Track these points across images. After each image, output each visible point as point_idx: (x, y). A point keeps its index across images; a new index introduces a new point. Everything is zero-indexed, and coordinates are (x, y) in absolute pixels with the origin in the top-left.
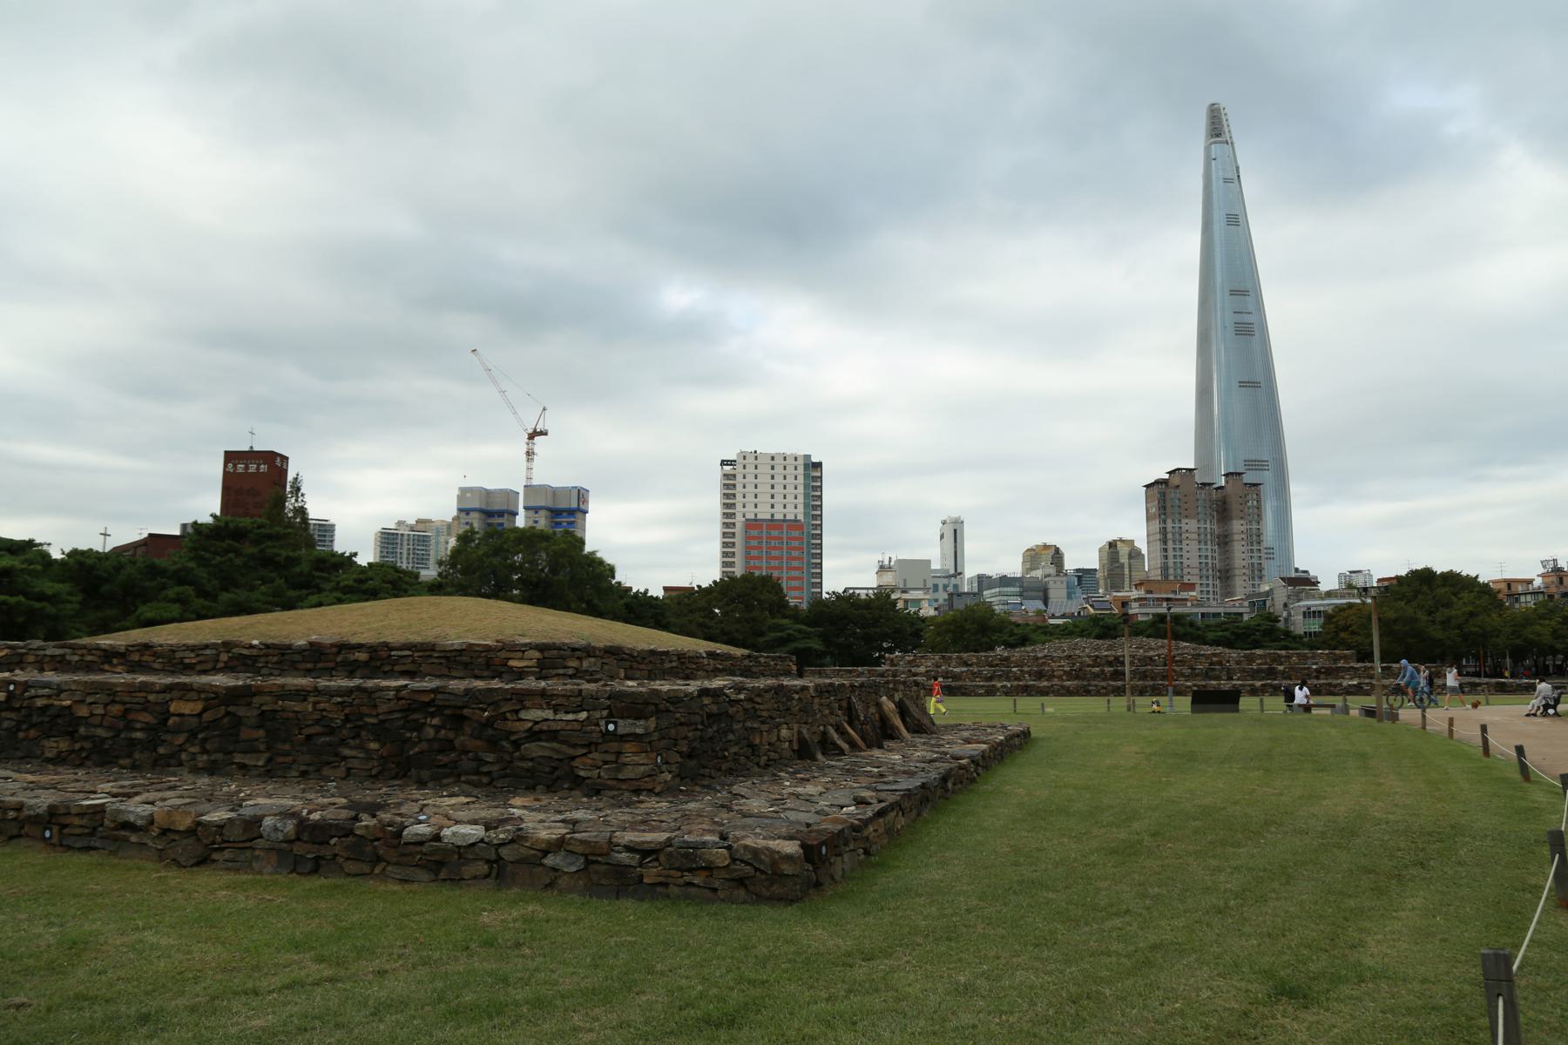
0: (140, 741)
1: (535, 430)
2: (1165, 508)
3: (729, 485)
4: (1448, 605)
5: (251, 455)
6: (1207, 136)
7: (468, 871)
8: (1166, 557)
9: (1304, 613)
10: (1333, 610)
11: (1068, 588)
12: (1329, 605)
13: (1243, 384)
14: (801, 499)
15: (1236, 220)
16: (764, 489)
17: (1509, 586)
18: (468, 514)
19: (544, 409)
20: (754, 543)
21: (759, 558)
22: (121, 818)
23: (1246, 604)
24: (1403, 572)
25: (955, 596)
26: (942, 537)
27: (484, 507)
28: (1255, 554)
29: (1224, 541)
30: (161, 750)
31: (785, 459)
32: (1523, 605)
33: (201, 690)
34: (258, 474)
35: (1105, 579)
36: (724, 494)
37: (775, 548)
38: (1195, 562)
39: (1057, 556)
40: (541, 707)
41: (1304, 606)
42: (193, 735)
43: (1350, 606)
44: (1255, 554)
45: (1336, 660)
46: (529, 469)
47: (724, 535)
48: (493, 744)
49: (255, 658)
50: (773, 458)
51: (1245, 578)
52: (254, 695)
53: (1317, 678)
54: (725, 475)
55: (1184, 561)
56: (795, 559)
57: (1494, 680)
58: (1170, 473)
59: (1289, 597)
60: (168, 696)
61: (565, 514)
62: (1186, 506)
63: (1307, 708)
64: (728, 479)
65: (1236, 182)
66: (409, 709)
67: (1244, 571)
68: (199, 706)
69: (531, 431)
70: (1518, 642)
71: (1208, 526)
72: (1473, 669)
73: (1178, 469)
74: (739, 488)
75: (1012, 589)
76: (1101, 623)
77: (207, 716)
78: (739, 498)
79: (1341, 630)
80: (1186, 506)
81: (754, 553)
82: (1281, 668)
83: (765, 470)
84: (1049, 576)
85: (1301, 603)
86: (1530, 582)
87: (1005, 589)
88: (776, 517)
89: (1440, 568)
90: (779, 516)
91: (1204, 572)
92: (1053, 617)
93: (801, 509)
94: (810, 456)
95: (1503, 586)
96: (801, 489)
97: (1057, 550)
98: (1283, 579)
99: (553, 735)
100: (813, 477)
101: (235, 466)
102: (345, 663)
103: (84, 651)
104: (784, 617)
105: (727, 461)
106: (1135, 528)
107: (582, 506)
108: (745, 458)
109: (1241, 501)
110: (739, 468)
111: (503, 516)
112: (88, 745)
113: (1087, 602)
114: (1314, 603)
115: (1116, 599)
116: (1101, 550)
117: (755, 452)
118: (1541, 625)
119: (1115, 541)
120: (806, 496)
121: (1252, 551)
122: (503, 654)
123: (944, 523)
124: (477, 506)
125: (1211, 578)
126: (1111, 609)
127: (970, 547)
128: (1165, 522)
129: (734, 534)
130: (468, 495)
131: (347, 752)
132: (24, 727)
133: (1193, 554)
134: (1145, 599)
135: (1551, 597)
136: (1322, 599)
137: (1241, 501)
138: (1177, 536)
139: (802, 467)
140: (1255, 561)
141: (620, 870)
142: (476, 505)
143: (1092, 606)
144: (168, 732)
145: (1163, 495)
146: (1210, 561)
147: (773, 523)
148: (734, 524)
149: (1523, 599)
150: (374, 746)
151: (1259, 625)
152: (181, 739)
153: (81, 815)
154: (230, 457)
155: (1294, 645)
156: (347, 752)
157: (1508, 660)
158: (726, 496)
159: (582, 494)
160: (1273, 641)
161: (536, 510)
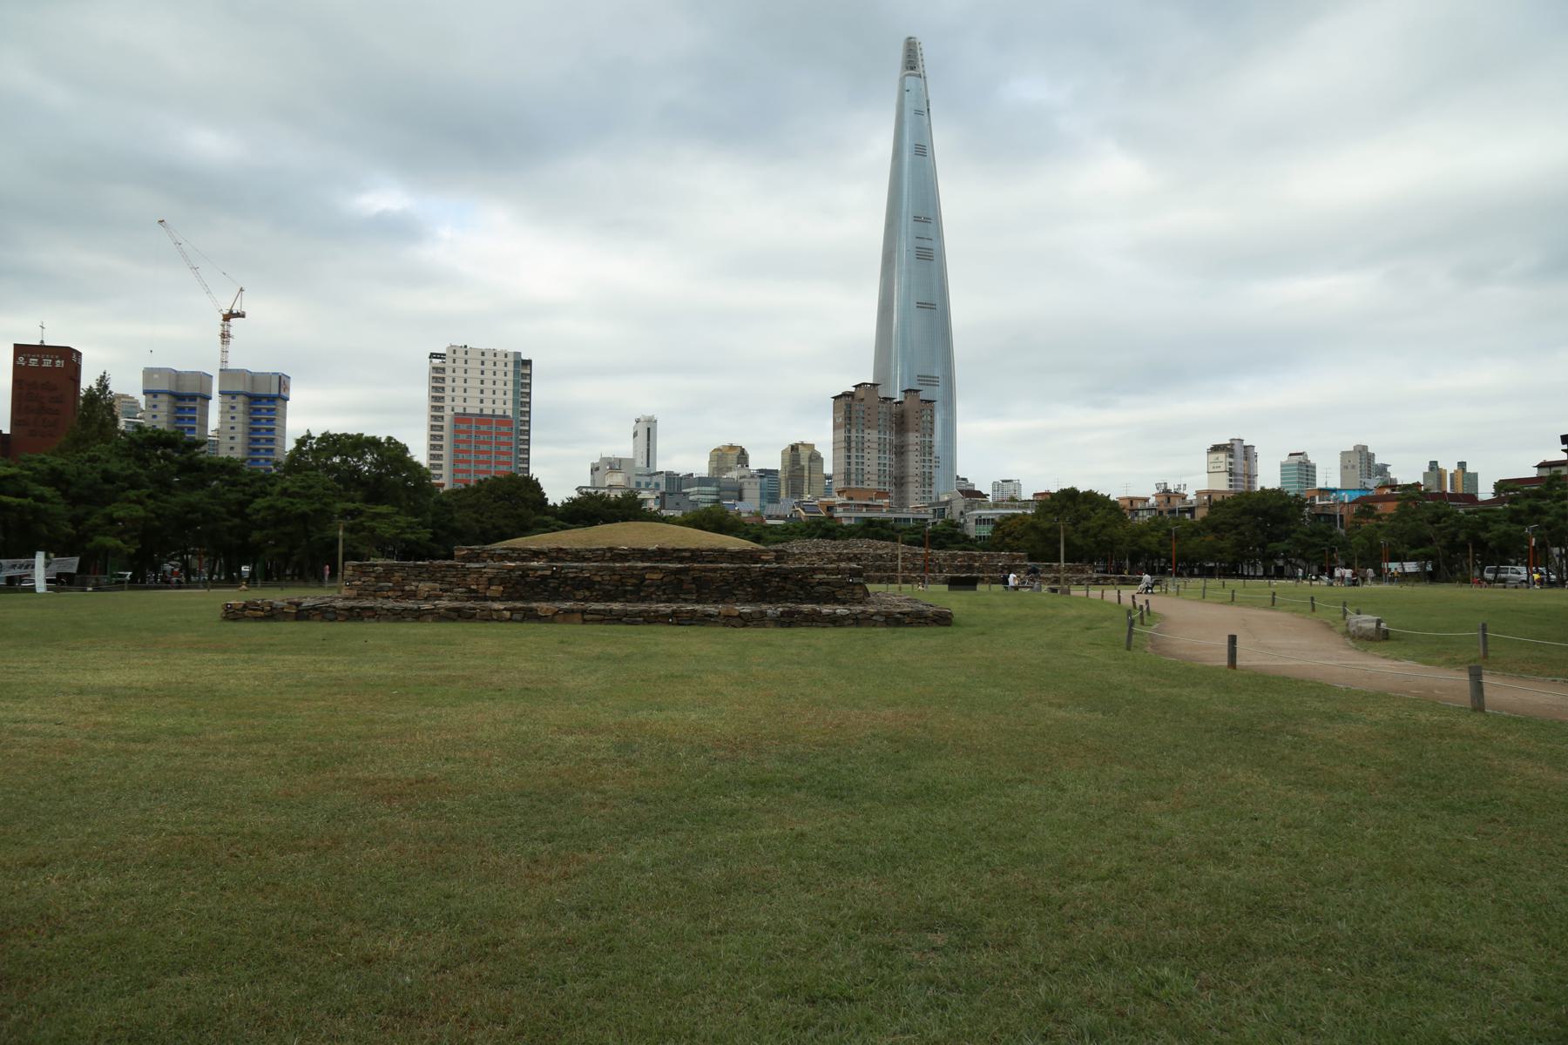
0: (631, 591)
1: (231, 312)
2: (850, 418)
3: (438, 379)
4: (1087, 518)
5: (41, 350)
6: (902, 68)
7: (846, 623)
8: (849, 464)
9: (976, 520)
10: (1000, 519)
11: (761, 489)
12: (996, 514)
13: (921, 305)
14: (510, 395)
15: (923, 150)
17: (1132, 502)
18: (155, 396)
19: (241, 290)
20: (463, 437)
21: (468, 452)
22: (707, 613)
23: (930, 511)
24: (1054, 490)
25: (666, 495)
26: (635, 435)
27: (174, 390)
28: (927, 464)
29: (900, 451)
30: (642, 594)
31: (495, 355)
33: (662, 570)
34: (53, 368)
35: (787, 480)
36: (433, 387)
37: (484, 443)
38: (874, 469)
39: (742, 457)
40: (821, 574)
41: (978, 514)
42: (658, 587)
43: (1014, 516)
44: (927, 464)
45: (1014, 559)
46: (224, 352)
47: (433, 427)
48: (801, 588)
49: (626, 555)
50: (483, 354)
51: (917, 485)
54: (434, 368)
55: (865, 467)
56: (504, 453)
57: (1118, 576)
58: (856, 386)
59: (966, 507)
60: (644, 572)
61: (264, 401)
62: (869, 418)
63: (1016, 588)
65: (926, 114)
66: (765, 575)
67: (917, 478)
68: (661, 576)
69: (226, 312)
70: (1135, 548)
71: (887, 437)
72: (1102, 569)
73: (864, 384)
74: (448, 381)
75: (709, 489)
76: (823, 526)
78: (448, 392)
80: (869, 418)
81: (463, 447)
82: (977, 564)
83: (474, 364)
84: (744, 477)
85: (974, 512)
86: (1146, 500)
87: (704, 488)
88: (485, 412)
89: (1082, 488)
90: (487, 411)
91: (882, 478)
92: (770, 517)
93: (510, 405)
94: (520, 353)
95: (1127, 503)
96: (510, 386)
97: (743, 451)
98: (961, 491)
99: (828, 584)
100: (523, 374)
101: (27, 359)
102: (677, 557)
103: (520, 552)
104: (546, 514)
106: (822, 436)
107: (283, 393)
108: (455, 352)
109: (917, 416)
110: (449, 362)
111: (195, 400)
112: (601, 593)
113: (799, 506)
114: (985, 513)
115: (822, 504)
116: (783, 453)
117: (466, 347)
118: (1153, 536)
120: (515, 392)
122: (758, 553)
123: (638, 421)
124: (167, 389)
125: (887, 483)
126: (819, 512)
127: (661, 444)
128: (849, 431)
129: (442, 427)
130: (156, 376)
131: (737, 592)
133: (874, 462)
134: (848, 505)
135: (1161, 513)
136: (991, 509)
137: (917, 416)
138: (860, 445)
140: (927, 470)
142: (166, 388)
143: (803, 509)
144: (645, 586)
145: (849, 406)
146: (887, 468)
147: (482, 418)
148: (442, 417)
149: (1141, 513)
150: (750, 589)
151: (944, 530)
152: (652, 589)
153: (687, 613)
154: (20, 350)
155: (971, 547)
156: (737, 592)
157: (1127, 561)
158: (435, 389)
159: (283, 381)
161: (233, 395)
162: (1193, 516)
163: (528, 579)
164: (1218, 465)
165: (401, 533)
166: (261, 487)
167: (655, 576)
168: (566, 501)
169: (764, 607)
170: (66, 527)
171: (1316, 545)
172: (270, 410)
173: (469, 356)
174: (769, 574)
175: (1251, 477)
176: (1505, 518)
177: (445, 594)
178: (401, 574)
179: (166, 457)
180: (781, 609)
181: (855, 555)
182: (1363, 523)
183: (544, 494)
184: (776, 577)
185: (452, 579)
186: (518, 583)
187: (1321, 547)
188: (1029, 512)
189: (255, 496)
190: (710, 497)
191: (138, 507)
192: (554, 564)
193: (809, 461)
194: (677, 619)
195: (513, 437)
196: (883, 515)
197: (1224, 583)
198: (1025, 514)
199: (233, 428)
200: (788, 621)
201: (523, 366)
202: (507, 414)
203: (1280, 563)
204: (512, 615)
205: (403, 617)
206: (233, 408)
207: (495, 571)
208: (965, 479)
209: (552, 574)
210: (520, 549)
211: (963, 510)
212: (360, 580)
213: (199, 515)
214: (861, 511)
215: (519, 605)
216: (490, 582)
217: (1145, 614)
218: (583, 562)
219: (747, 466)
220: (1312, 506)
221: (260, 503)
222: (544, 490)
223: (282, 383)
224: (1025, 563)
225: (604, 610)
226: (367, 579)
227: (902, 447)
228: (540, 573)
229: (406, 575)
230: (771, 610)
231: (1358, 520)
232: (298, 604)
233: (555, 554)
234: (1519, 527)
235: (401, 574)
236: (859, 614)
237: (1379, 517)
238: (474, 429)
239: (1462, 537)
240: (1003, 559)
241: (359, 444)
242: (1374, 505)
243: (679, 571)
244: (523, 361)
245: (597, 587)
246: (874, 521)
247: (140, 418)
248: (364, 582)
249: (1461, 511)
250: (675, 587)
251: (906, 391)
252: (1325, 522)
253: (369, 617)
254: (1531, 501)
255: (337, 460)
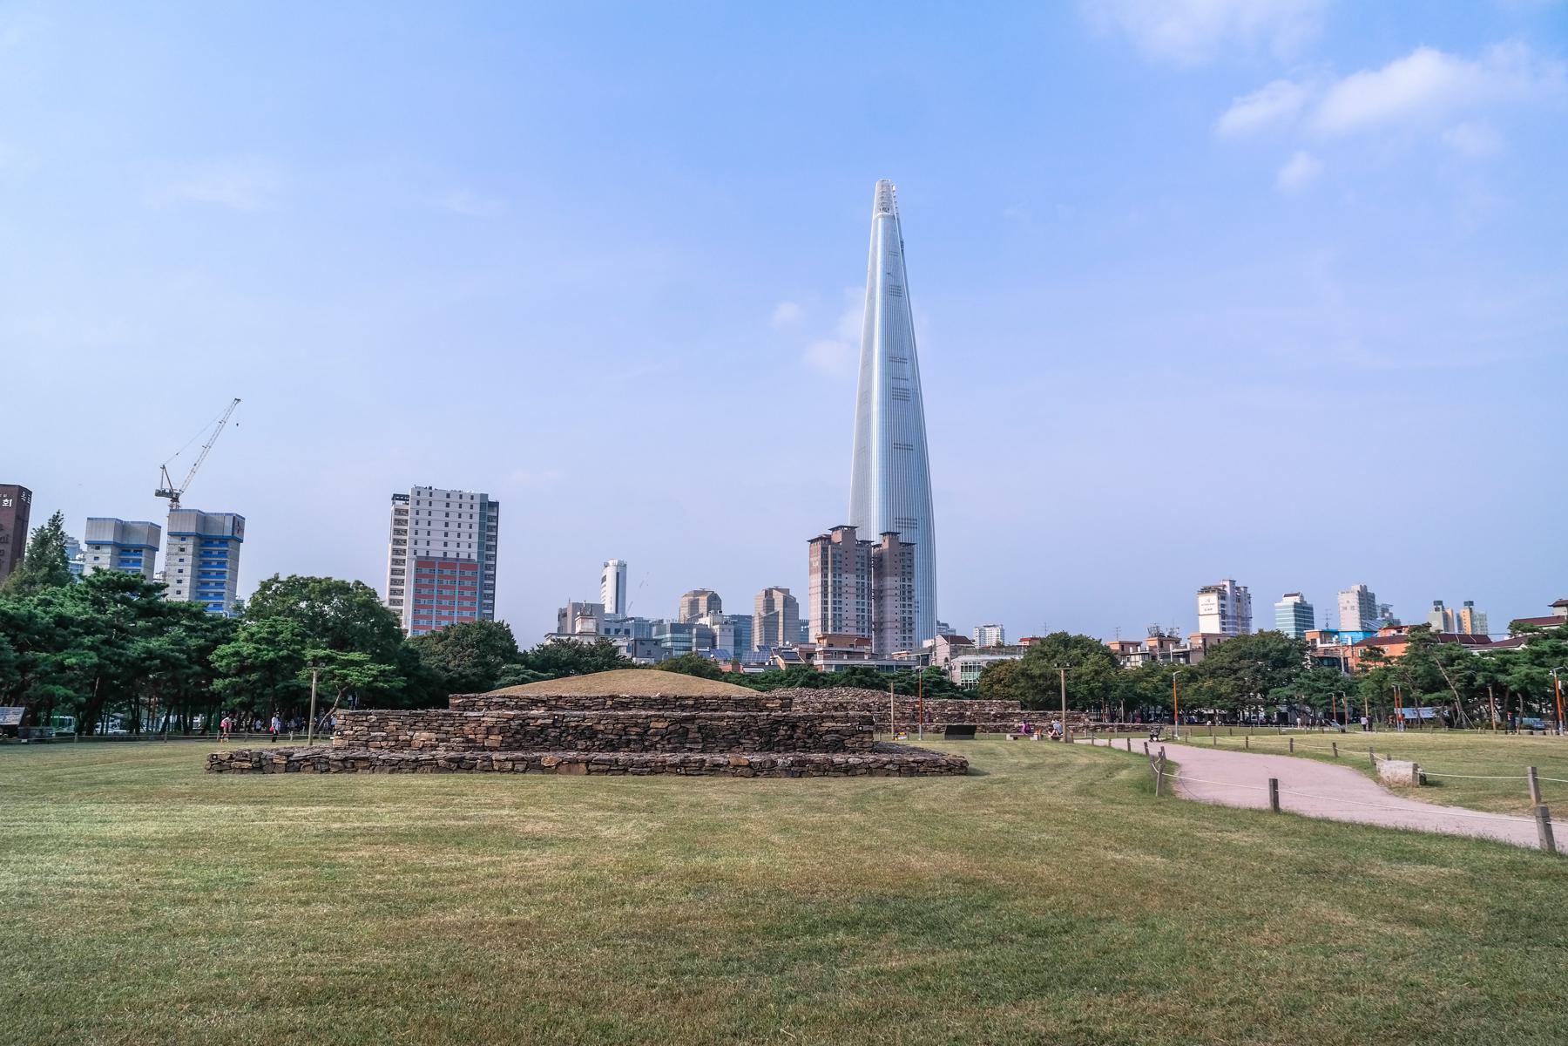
0: (634, 740)
7: (858, 772)
16: (438, 526)
24: (1043, 635)
28: (907, 609)
31: (461, 497)
32: (1133, 664)
39: (714, 601)
43: (1003, 662)
44: (907, 609)
49: (628, 704)
50: (448, 496)
52: (696, 719)
53: (994, 721)
54: (396, 510)
55: (843, 613)
61: (216, 542)
64: (400, 514)
68: (666, 724)
70: (1130, 695)
75: (682, 635)
77: (671, 728)
79: (995, 683)
82: (968, 713)
83: (439, 506)
89: (1073, 633)
92: (747, 666)
93: (475, 548)
102: (680, 705)
104: (516, 662)
105: (400, 495)
107: (236, 535)
108: (419, 493)
114: (970, 659)
117: (430, 488)
119: (771, 589)
121: (904, 606)
131: (744, 741)
132: (564, 735)
139: (479, 506)
140: (906, 615)
141: (912, 769)
145: (824, 550)
147: (445, 562)
151: (930, 678)
152: (658, 738)
153: (695, 763)
156: (744, 741)
160: (941, 691)
161: (183, 537)
162: (1188, 662)
163: (528, 728)
164: (1209, 607)
165: (372, 682)
166: (223, 633)
167: (660, 725)
168: (537, 648)
169: (774, 756)
170: (13, 674)
171: (1320, 691)
172: (222, 553)
173: (434, 497)
174: (777, 722)
175: (1245, 620)
176: (1525, 660)
177: (441, 744)
178: (395, 723)
179: (124, 601)
180: (791, 758)
181: (841, 704)
182: (1371, 666)
183: (515, 642)
184: (784, 726)
185: (449, 729)
186: (517, 732)
187: (1327, 692)
188: (1017, 658)
189: (217, 642)
190: (682, 644)
191: (92, 654)
192: (555, 713)
193: (784, 607)
194: (682, 768)
195: (478, 581)
196: (866, 661)
197: (1231, 730)
198: (1013, 660)
199: (181, 571)
200: (798, 770)
201: (488, 510)
202: (472, 558)
203: (1284, 709)
204: (514, 765)
205: (400, 769)
206: (182, 550)
207: (495, 719)
208: (946, 625)
209: (553, 723)
210: (518, 697)
211: (949, 657)
212: (352, 730)
213: (158, 661)
214: (842, 659)
215: (520, 754)
216: (489, 731)
217: (1166, 765)
218: (582, 710)
219: (721, 612)
220: (1314, 649)
221: (224, 649)
222: (515, 638)
223: (236, 524)
224: (1018, 711)
225: (609, 760)
226: (360, 728)
227: (881, 591)
228: (539, 722)
229: (400, 724)
230: (782, 759)
231: (1366, 663)
232: (289, 755)
233: (554, 703)
234: (1542, 670)
235: (395, 723)
236: (871, 763)
237: (1387, 660)
238: (458, 574)
239: (1480, 680)
240: (994, 707)
241: (330, 589)
242: (1382, 647)
243: (686, 719)
244: (490, 503)
245: (600, 736)
246: (857, 669)
247: (80, 560)
248: (356, 731)
249: (1476, 653)
250: (678, 736)
251: (884, 534)
252: (1328, 666)
253: (364, 768)
254: (1553, 641)
255: (303, 605)
